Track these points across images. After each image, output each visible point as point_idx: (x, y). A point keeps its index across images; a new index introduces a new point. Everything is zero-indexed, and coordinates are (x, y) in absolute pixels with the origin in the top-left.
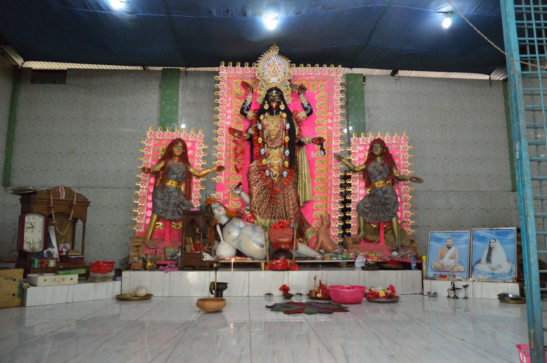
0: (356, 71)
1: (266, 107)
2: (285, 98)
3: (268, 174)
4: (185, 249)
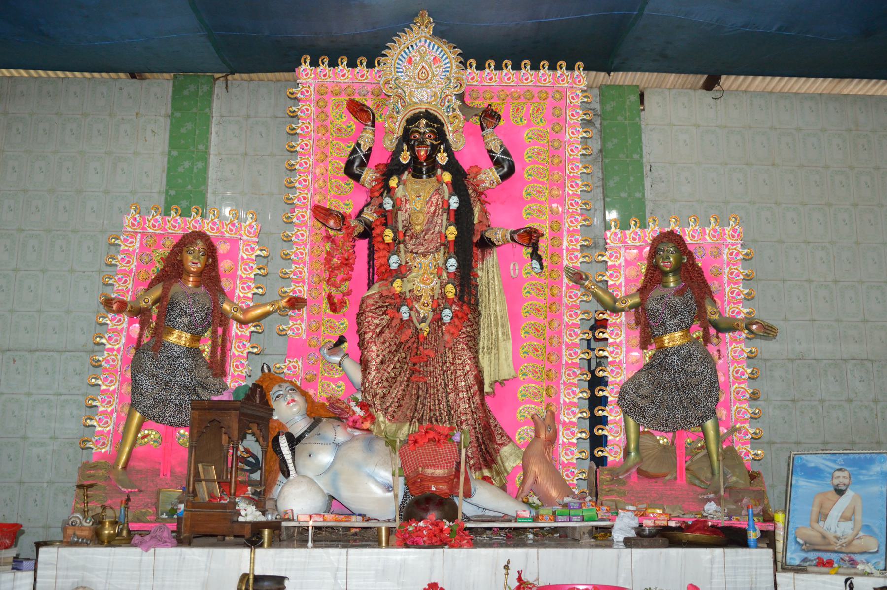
0: (621, 78)
1: (405, 158)
2: (450, 137)
3: (405, 317)
4: (194, 493)
